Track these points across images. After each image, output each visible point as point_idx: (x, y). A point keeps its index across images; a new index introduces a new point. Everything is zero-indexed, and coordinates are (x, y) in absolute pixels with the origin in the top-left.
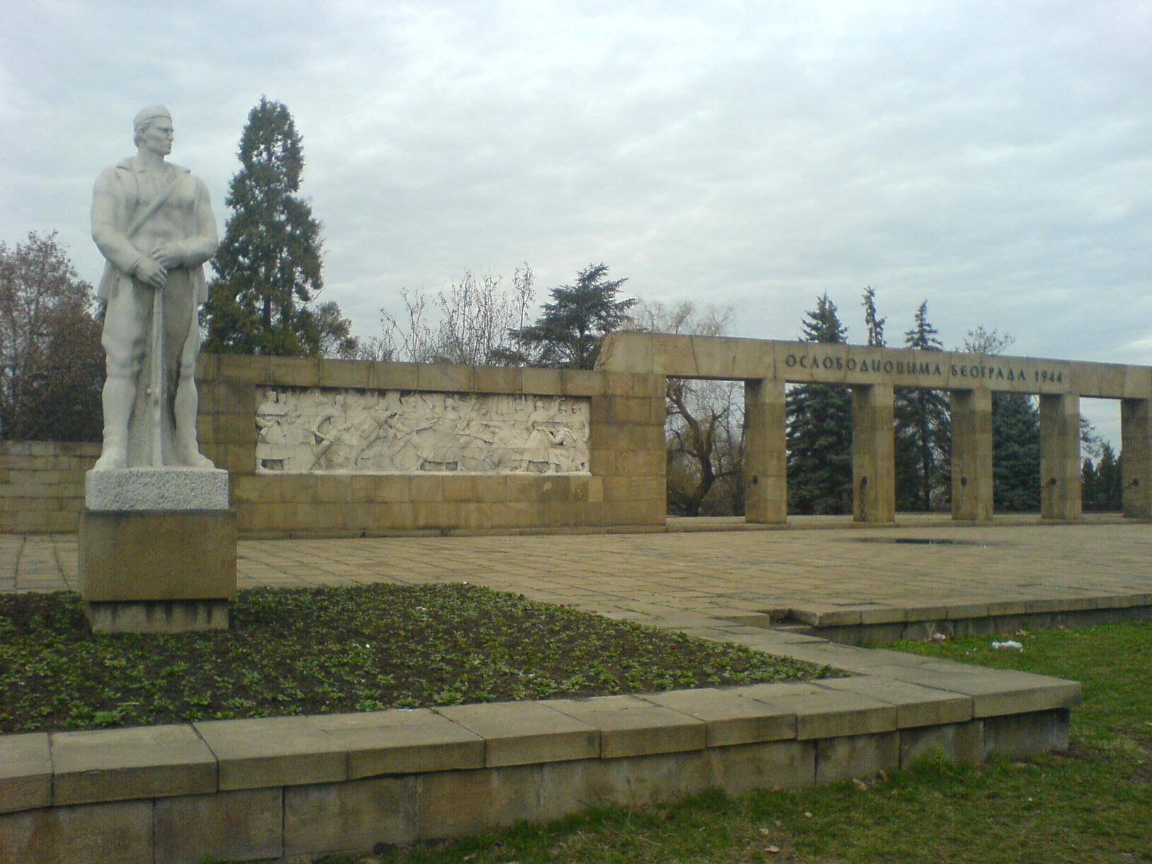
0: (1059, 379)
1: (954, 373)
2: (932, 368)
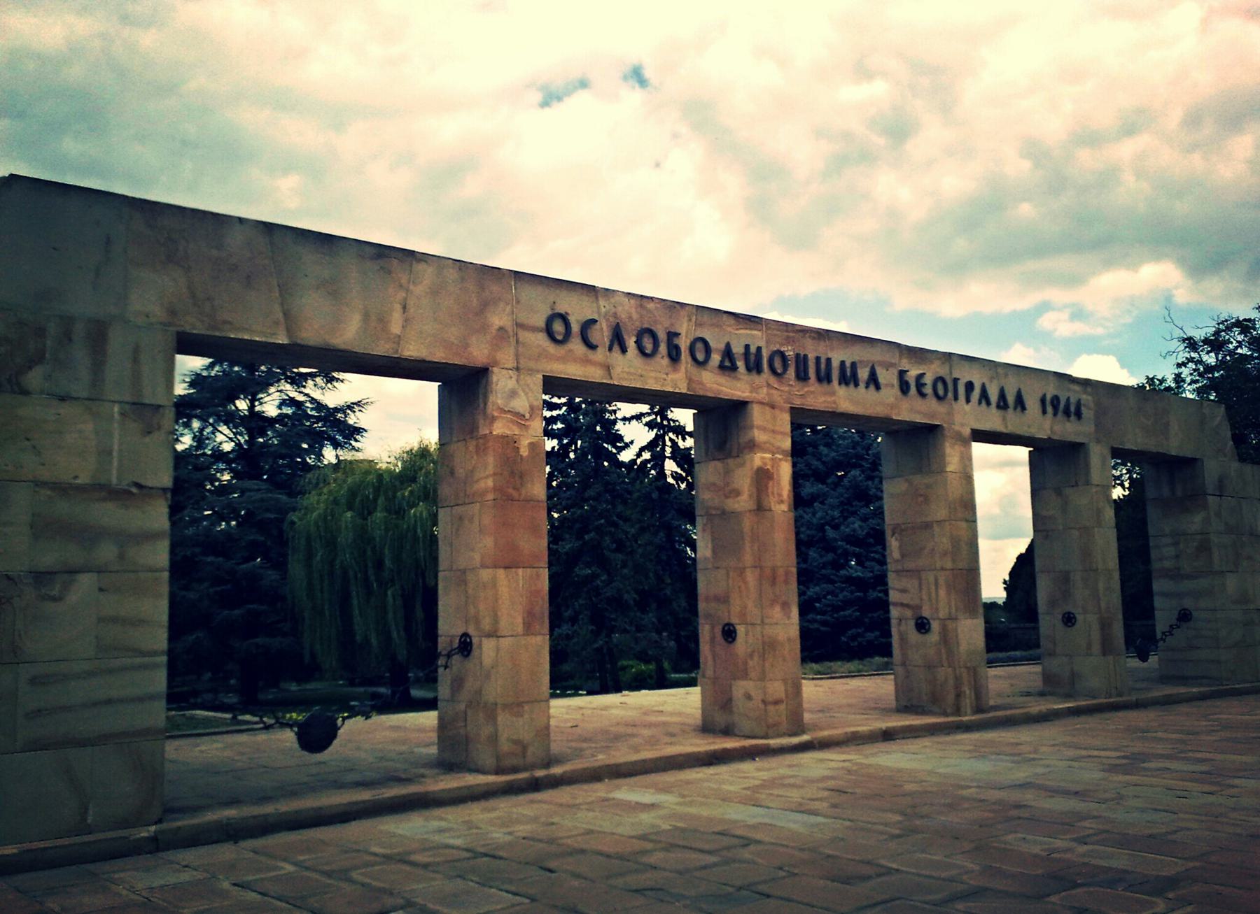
0: (1078, 414)
1: (904, 387)
2: (863, 374)
